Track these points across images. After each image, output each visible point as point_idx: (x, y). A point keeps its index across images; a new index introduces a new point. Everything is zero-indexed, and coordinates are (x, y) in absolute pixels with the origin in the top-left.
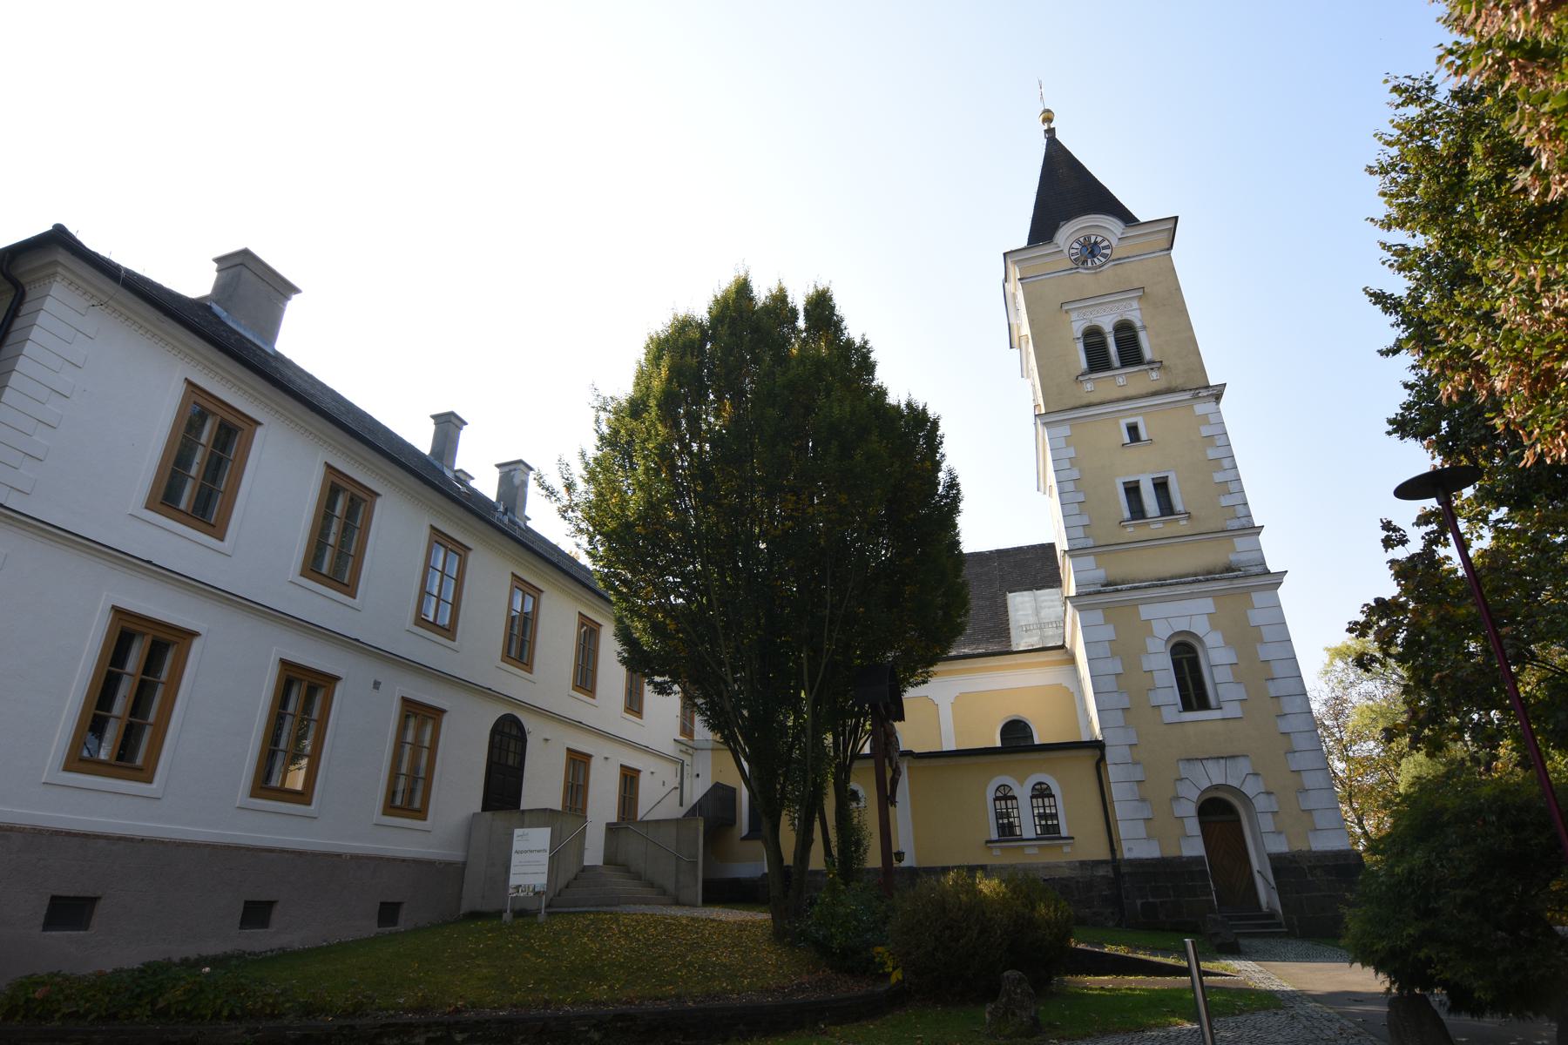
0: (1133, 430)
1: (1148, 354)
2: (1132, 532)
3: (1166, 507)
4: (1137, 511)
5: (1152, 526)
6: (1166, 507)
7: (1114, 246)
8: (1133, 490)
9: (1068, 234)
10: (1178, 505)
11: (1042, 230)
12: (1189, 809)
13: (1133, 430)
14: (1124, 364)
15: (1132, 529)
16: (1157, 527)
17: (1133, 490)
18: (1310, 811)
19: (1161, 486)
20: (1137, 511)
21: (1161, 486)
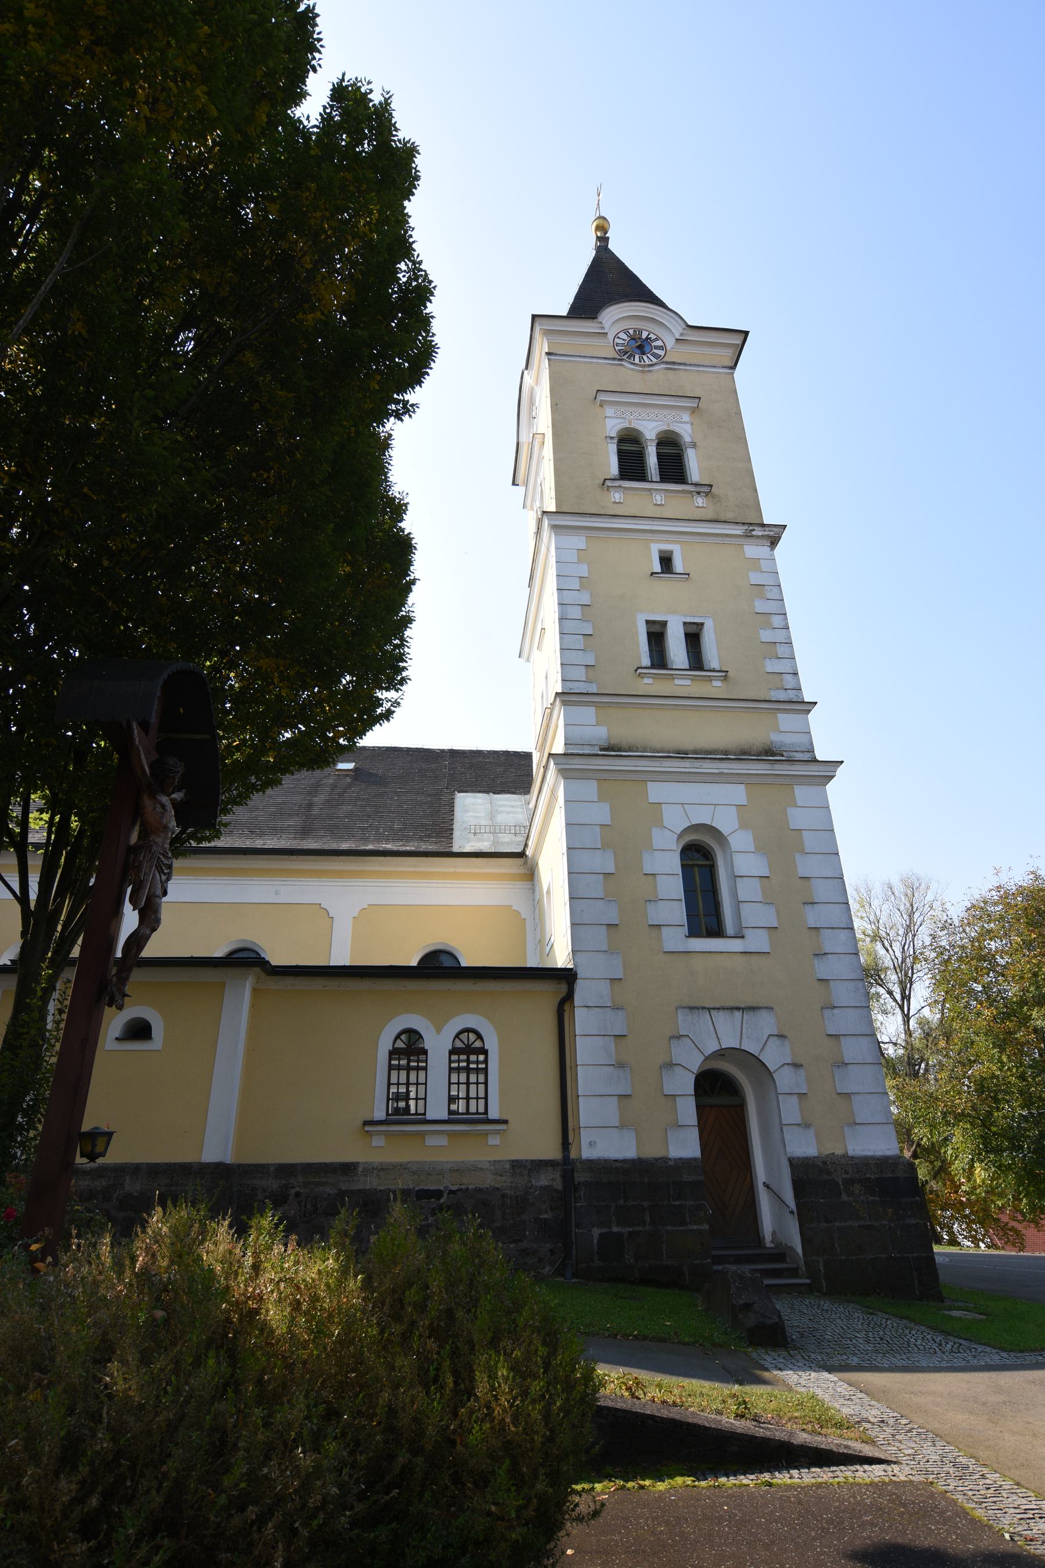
0: (666, 561)
2: (648, 684)
4: (659, 657)
5: (677, 682)
7: (668, 348)
8: (657, 635)
13: (666, 561)
15: (650, 681)
16: (684, 685)
17: (657, 635)
18: (623, 1126)
19: (693, 637)
20: (659, 657)
21: (693, 637)
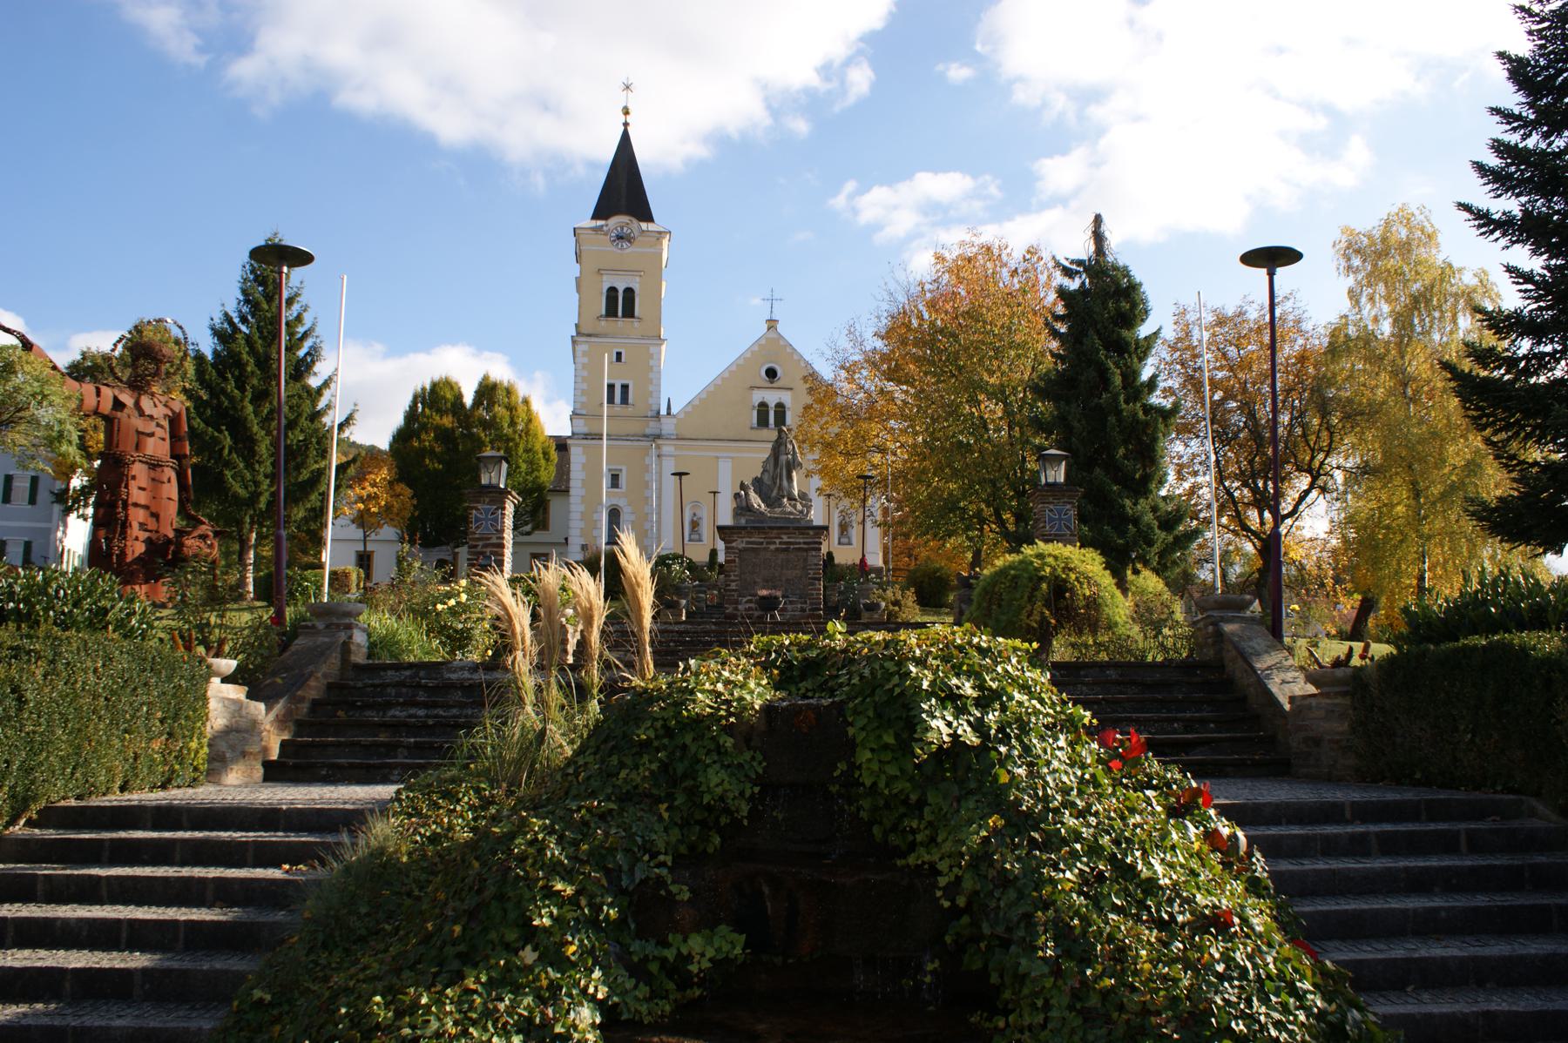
0: (619, 355)
1: (636, 313)
3: (625, 400)
6: (625, 400)
9: (616, 222)
10: (630, 401)
11: (601, 212)
12: (605, 291)
13: (619, 355)
14: (624, 316)
16: (618, 407)
19: (625, 388)
21: (625, 388)
